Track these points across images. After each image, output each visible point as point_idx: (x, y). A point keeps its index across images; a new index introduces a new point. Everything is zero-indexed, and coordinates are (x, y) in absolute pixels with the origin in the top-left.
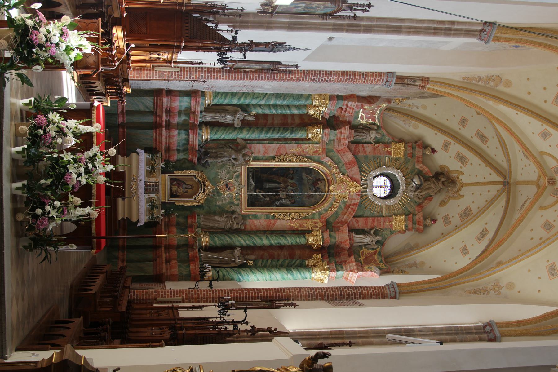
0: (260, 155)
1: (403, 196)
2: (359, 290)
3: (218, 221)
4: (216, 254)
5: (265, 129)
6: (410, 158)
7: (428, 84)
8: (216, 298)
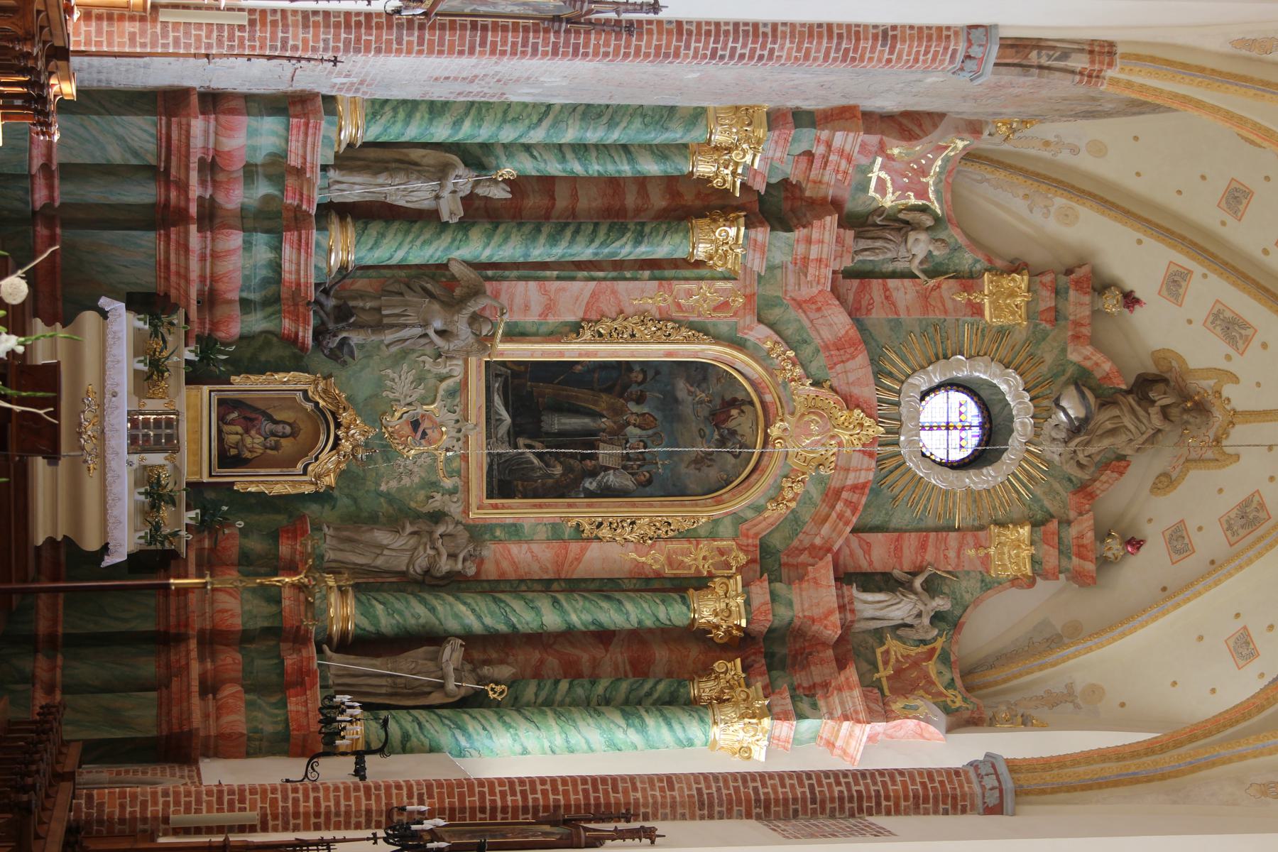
0: (530, 319)
1: (1025, 459)
2: (875, 783)
4: (378, 661)
5: (546, 230)
6: (1048, 327)
7: (1110, 65)
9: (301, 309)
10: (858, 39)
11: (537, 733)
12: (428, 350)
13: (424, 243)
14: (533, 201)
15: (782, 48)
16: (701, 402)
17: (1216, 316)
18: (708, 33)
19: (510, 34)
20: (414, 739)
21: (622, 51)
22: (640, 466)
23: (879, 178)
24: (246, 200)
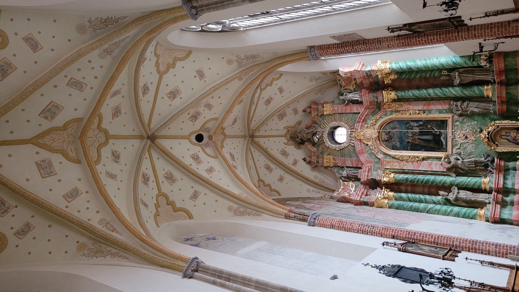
0: (435, 162)
1: (325, 128)
2: (339, 51)
3: (476, 107)
4: (477, 79)
5: (430, 183)
6: (320, 155)
7: (286, 214)
8: (471, 30)
9: (498, 167)
10: (339, 226)
11: (434, 63)
12: (462, 156)
13: (462, 182)
14: (433, 190)
15: (357, 227)
16: (394, 141)
17: (199, 162)
18: (374, 233)
19: (427, 240)
20: (467, 59)
21: (397, 231)
22: (409, 127)
23: (352, 188)
24: (514, 196)
